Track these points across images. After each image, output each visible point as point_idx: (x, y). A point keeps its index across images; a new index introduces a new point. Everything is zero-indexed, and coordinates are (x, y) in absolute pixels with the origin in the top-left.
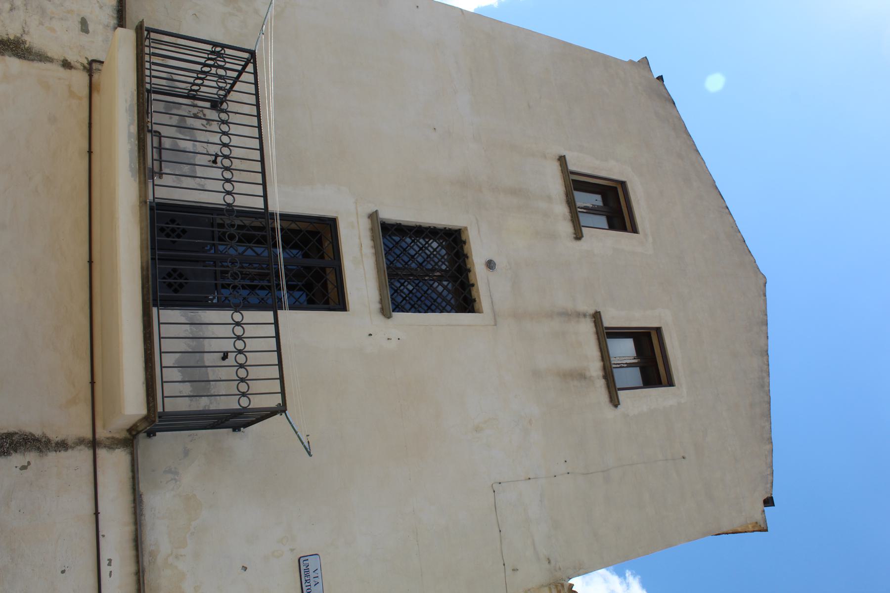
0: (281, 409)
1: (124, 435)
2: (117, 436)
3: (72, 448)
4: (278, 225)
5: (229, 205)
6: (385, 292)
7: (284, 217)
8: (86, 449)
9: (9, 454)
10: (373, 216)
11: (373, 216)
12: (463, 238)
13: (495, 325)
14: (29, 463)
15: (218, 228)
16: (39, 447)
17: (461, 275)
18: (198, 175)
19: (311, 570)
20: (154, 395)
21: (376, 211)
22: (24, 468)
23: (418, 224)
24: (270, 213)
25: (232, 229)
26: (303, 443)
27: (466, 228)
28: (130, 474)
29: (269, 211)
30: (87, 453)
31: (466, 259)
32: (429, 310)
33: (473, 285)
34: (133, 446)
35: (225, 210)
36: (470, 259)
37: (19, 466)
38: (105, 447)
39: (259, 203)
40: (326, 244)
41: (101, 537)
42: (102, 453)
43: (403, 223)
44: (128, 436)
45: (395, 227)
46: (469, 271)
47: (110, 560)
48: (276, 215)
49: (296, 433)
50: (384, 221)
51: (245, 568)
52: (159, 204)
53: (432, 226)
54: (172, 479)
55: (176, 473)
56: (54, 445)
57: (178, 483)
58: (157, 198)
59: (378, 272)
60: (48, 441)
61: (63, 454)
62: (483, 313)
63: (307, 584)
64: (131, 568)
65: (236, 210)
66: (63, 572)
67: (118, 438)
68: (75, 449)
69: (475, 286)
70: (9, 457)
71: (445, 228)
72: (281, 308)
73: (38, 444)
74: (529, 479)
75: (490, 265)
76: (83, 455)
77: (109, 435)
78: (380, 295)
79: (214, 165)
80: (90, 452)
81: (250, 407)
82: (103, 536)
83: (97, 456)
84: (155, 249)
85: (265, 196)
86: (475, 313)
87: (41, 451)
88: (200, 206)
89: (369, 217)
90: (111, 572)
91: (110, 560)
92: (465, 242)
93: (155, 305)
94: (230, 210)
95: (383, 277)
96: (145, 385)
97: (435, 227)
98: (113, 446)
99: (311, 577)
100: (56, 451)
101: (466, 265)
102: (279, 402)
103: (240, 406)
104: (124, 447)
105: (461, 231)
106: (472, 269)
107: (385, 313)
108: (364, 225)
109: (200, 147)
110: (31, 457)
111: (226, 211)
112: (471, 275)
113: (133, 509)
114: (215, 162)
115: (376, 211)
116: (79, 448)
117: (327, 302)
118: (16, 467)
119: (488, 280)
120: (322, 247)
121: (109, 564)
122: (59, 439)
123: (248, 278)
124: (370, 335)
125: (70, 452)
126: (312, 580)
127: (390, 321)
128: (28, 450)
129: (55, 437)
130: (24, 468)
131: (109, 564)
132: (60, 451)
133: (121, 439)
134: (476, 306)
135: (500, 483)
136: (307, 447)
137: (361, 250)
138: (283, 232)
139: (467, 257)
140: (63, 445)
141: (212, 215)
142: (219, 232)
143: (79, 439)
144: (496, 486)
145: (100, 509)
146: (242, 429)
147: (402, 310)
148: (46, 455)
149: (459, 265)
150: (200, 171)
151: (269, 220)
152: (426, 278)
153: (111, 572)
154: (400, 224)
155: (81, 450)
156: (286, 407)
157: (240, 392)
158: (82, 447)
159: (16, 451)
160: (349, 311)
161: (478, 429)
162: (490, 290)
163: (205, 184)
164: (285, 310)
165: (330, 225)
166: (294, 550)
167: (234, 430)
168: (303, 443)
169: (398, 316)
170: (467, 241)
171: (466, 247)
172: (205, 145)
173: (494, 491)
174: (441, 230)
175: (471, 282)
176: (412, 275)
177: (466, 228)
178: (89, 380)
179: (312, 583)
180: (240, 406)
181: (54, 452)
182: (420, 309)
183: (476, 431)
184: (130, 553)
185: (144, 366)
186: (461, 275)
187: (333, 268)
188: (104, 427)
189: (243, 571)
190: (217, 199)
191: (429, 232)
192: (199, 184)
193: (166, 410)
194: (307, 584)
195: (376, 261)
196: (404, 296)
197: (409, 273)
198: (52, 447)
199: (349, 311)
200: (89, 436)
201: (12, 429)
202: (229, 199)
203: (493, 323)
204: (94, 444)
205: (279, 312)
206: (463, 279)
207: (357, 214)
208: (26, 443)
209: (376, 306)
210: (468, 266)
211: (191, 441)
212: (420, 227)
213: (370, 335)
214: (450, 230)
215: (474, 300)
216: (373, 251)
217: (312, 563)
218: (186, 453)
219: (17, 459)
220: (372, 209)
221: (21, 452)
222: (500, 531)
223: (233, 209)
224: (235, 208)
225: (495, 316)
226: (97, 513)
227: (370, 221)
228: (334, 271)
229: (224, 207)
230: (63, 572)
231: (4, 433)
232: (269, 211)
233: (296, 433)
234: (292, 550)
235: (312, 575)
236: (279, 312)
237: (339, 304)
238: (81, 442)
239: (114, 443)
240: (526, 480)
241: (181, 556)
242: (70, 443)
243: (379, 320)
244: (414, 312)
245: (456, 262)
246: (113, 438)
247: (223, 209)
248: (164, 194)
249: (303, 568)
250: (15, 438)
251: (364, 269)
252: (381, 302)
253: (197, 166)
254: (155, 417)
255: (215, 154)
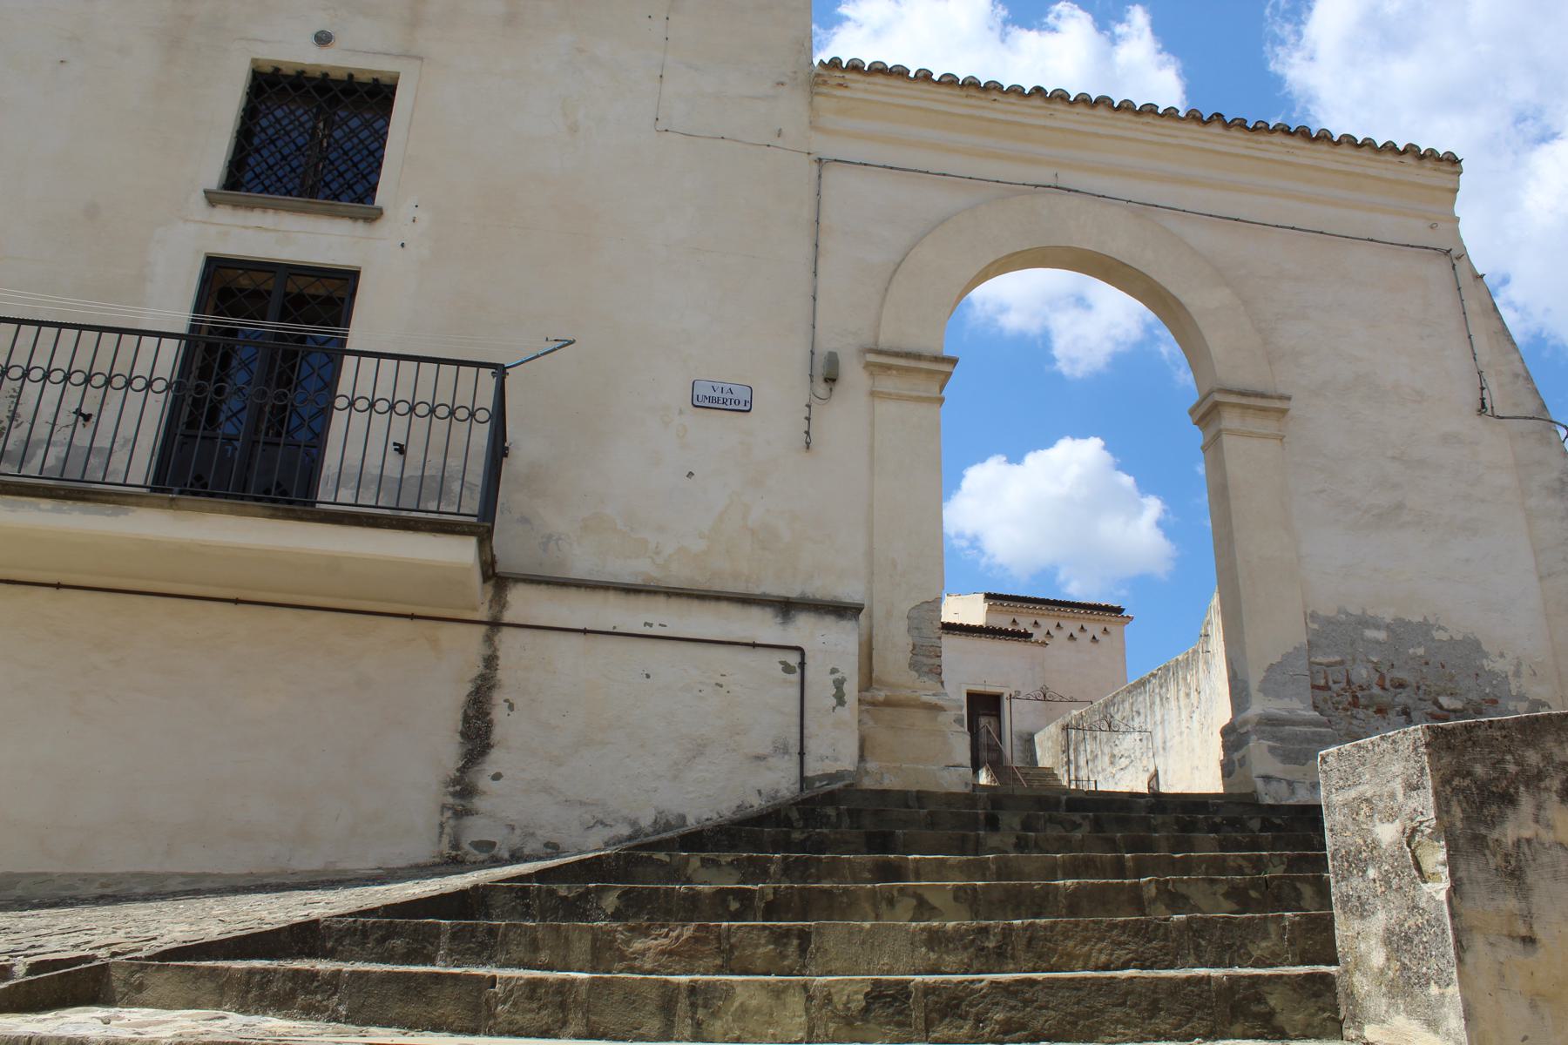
0: (500, 371)
1: (489, 589)
2: (489, 596)
3: (496, 650)
4: (209, 317)
5: (168, 387)
6: (341, 208)
7: (199, 307)
8: (500, 634)
9: (491, 722)
10: (212, 199)
11: (212, 199)
12: (269, 69)
13: (421, 59)
14: (506, 701)
15: (198, 428)
16: (489, 688)
17: (331, 90)
18: (108, 445)
19: (710, 393)
20: (453, 524)
21: (206, 192)
22: (511, 707)
23: (235, 135)
24: (190, 332)
25: (208, 389)
26: (554, 350)
27: (254, 61)
28: (543, 587)
29: (187, 333)
30: (506, 635)
31: (305, 75)
32: (384, 137)
33: (351, 76)
34: (507, 578)
35: (177, 394)
36: (308, 70)
37: (508, 711)
38: (501, 612)
39: (170, 348)
40: (245, 282)
41: (615, 631)
42: (508, 617)
43: (229, 158)
44: (492, 582)
45: (234, 170)
46: (326, 75)
47: (646, 624)
48: (196, 321)
49: (538, 356)
50: (221, 185)
51: (691, 474)
52: (157, 479)
53: (241, 113)
54: (557, 544)
55: (550, 537)
56: (488, 671)
57: (563, 537)
58: (146, 483)
59: (306, 213)
60: (483, 677)
61: (501, 662)
62: (399, 73)
63: (728, 403)
64: (661, 601)
65: (178, 377)
66: (648, 676)
67: (493, 596)
68: (498, 647)
69: (353, 72)
70: (495, 721)
71: (247, 93)
72: (344, 342)
73: (484, 689)
74: (661, 76)
75: (323, 39)
76: (506, 638)
77: (487, 605)
78: (343, 217)
79: (94, 419)
80: (505, 630)
81: (491, 411)
82: (614, 628)
83: (511, 622)
84: (227, 495)
85: (161, 335)
86: (396, 85)
87: (494, 686)
88: (182, 358)
89: (213, 206)
90: (660, 625)
91: (646, 624)
92: (277, 70)
93: (313, 504)
94: (177, 387)
95: (318, 207)
96: (438, 535)
97: (244, 110)
98: (502, 603)
99: (722, 396)
100: (496, 669)
101: (314, 79)
102: (490, 373)
103: (487, 421)
104: (506, 590)
105: (256, 70)
106: (324, 71)
107: (374, 216)
108: (225, 216)
109: (62, 436)
110: (498, 698)
111: (178, 392)
112: (334, 75)
113: (588, 590)
114: (87, 418)
115: (206, 192)
116: (497, 642)
117: (342, 300)
118: (509, 715)
119: (349, 50)
120: (246, 290)
121: (651, 625)
122: (481, 665)
123: (290, 373)
124: (403, 245)
125: (499, 654)
126: (724, 395)
127: (387, 213)
128: (489, 700)
129: (477, 668)
130: (511, 707)
131: (651, 625)
132: (497, 665)
133: (495, 592)
134: (385, 80)
135: (657, 119)
136: (561, 343)
137: (266, 230)
138: (225, 311)
139: (303, 72)
140: (490, 661)
141: (176, 434)
142: (205, 429)
143: (486, 641)
144: (660, 126)
145: (582, 627)
146: (506, 445)
147: (373, 189)
148: (499, 681)
149: (314, 87)
150: (103, 441)
151: (201, 335)
152: (325, 144)
153: (660, 625)
154: (230, 162)
155: (500, 641)
156: (499, 364)
157: (467, 419)
158: (496, 639)
159: (489, 714)
160: (360, 268)
161: (574, 129)
162: (365, 52)
163: (124, 437)
164: (347, 335)
165: (220, 267)
166: (680, 410)
167: (506, 455)
168: (554, 350)
169: (381, 198)
170: (275, 65)
171: (286, 70)
172: (56, 428)
173: (667, 131)
174: (249, 101)
175: (346, 78)
176: (316, 165)
177: (254, 61)
178: (407, 621)
179: (729, 396)
180: (487, 421)
181: (498, 671)
182: (381, 132)
183: (575, 132)
184: (642, 600)
185: (411, 532)
186: (331, 90)
187: (288, 277)
188: (475, 609)
189: (693, 477)
190: (157, 405)
191: (256, 98)
192: (124, 445)
193: (476, 512)
194: (728, 403)
195: (288, 211)
196: (366, 143)
197: (313, 169)
198: (490, 673)
199: (360, 268)
200: (483, 629)
201: (459, 716)
202: (159, 385)
203: (419, 62)
204: (495, 624)
205: (348, 347)
206: (339, 88)
207: (205, 223)
208: (480, 702)
209: (360, 228)
210: (318, 74)
211: (510, 512)
212: (231, 163)
213: (403, 245)
214: (251, 87)
215: (376, 80)
216: (271, 212)
217: (704, 390)
218: (525, 520)
219: (499, 713)
220: (199, 199)
221: (490, 709)
222: (723, 138)
223: (175, 382)
224: (175, 378)
225: (405, 56)
226: (585, 631)
227: (221, 206)
228: (292, 277)
229: (171, 395)
230: (648, 676)
231: (463, 725)
232: (187, 333)
233: (538, 356)
234: (681, 412)
235: (717, 394)
236: (348, 347)
237: (348, 280)
238: (489, 640)
239: (499, 600)
240: (661, 82)
241: (657, 547)
242: (489, 652)
243: (381, 227)
244: (379, 175)
245: (308, 91)
246: (491, 601)
247: (174, 395)
248: (141, 470)
249: (706, 404)
250: (471, 713)
251: (299, 232)
252: (354, 218)
253: (94, 445)
254: (483, 526)
255: (75, 416)
